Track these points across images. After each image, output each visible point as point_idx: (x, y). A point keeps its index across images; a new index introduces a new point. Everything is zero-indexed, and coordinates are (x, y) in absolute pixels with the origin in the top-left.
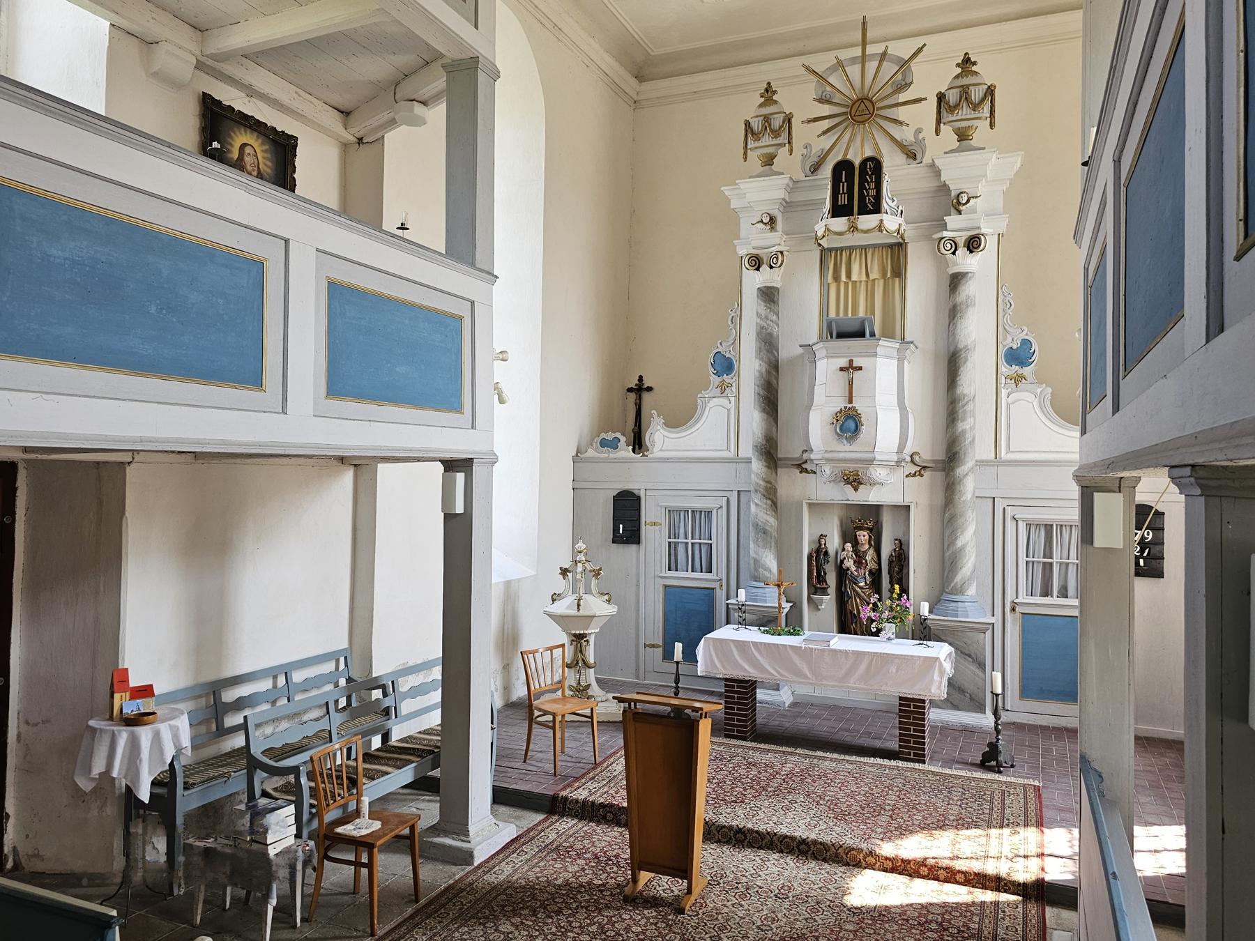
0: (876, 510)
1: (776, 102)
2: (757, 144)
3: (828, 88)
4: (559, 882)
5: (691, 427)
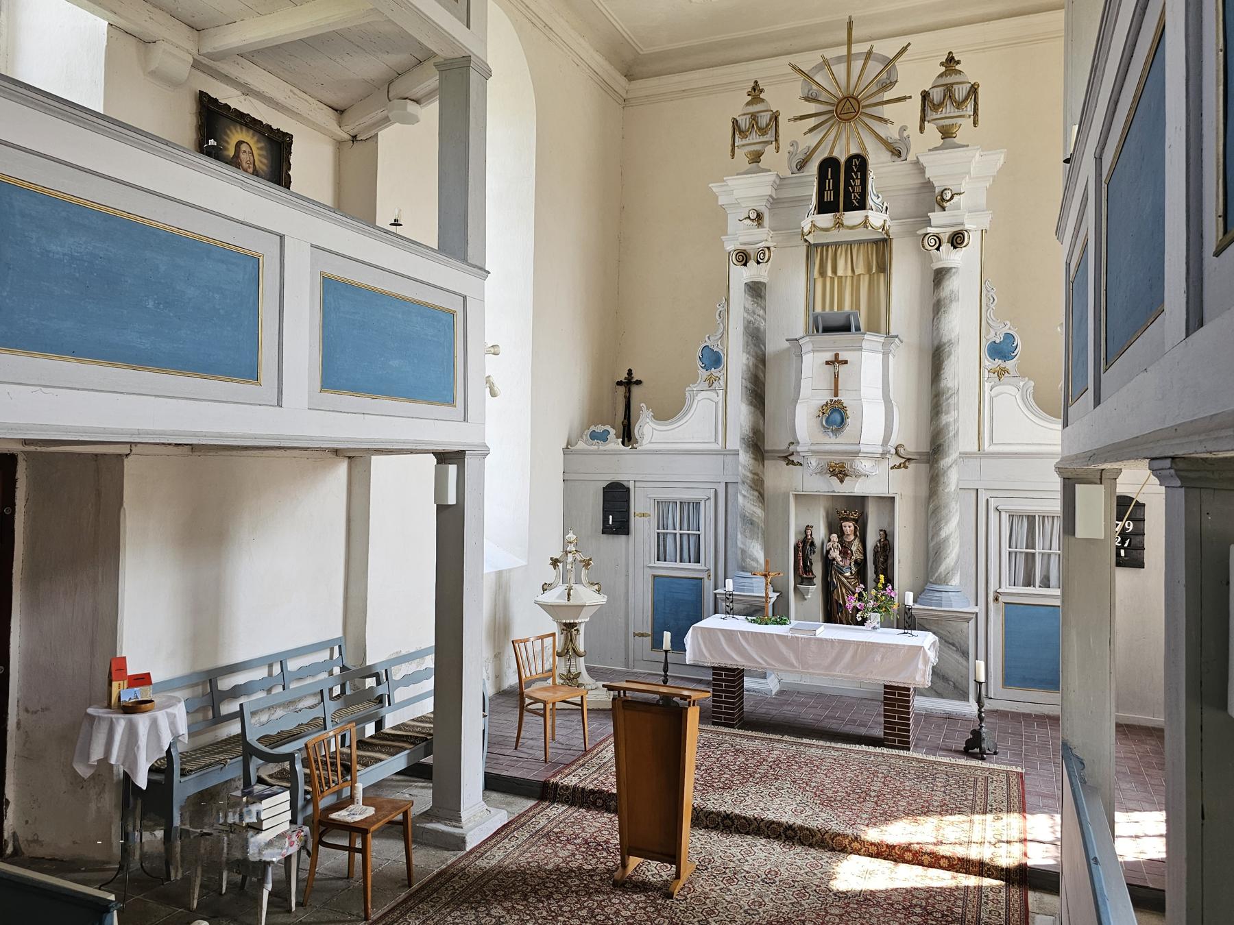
0: (861, 501)
1: (763, 100)
2: (745, 142)
3: (815, 87)
4: (550, 867)
5: (679, 419)
